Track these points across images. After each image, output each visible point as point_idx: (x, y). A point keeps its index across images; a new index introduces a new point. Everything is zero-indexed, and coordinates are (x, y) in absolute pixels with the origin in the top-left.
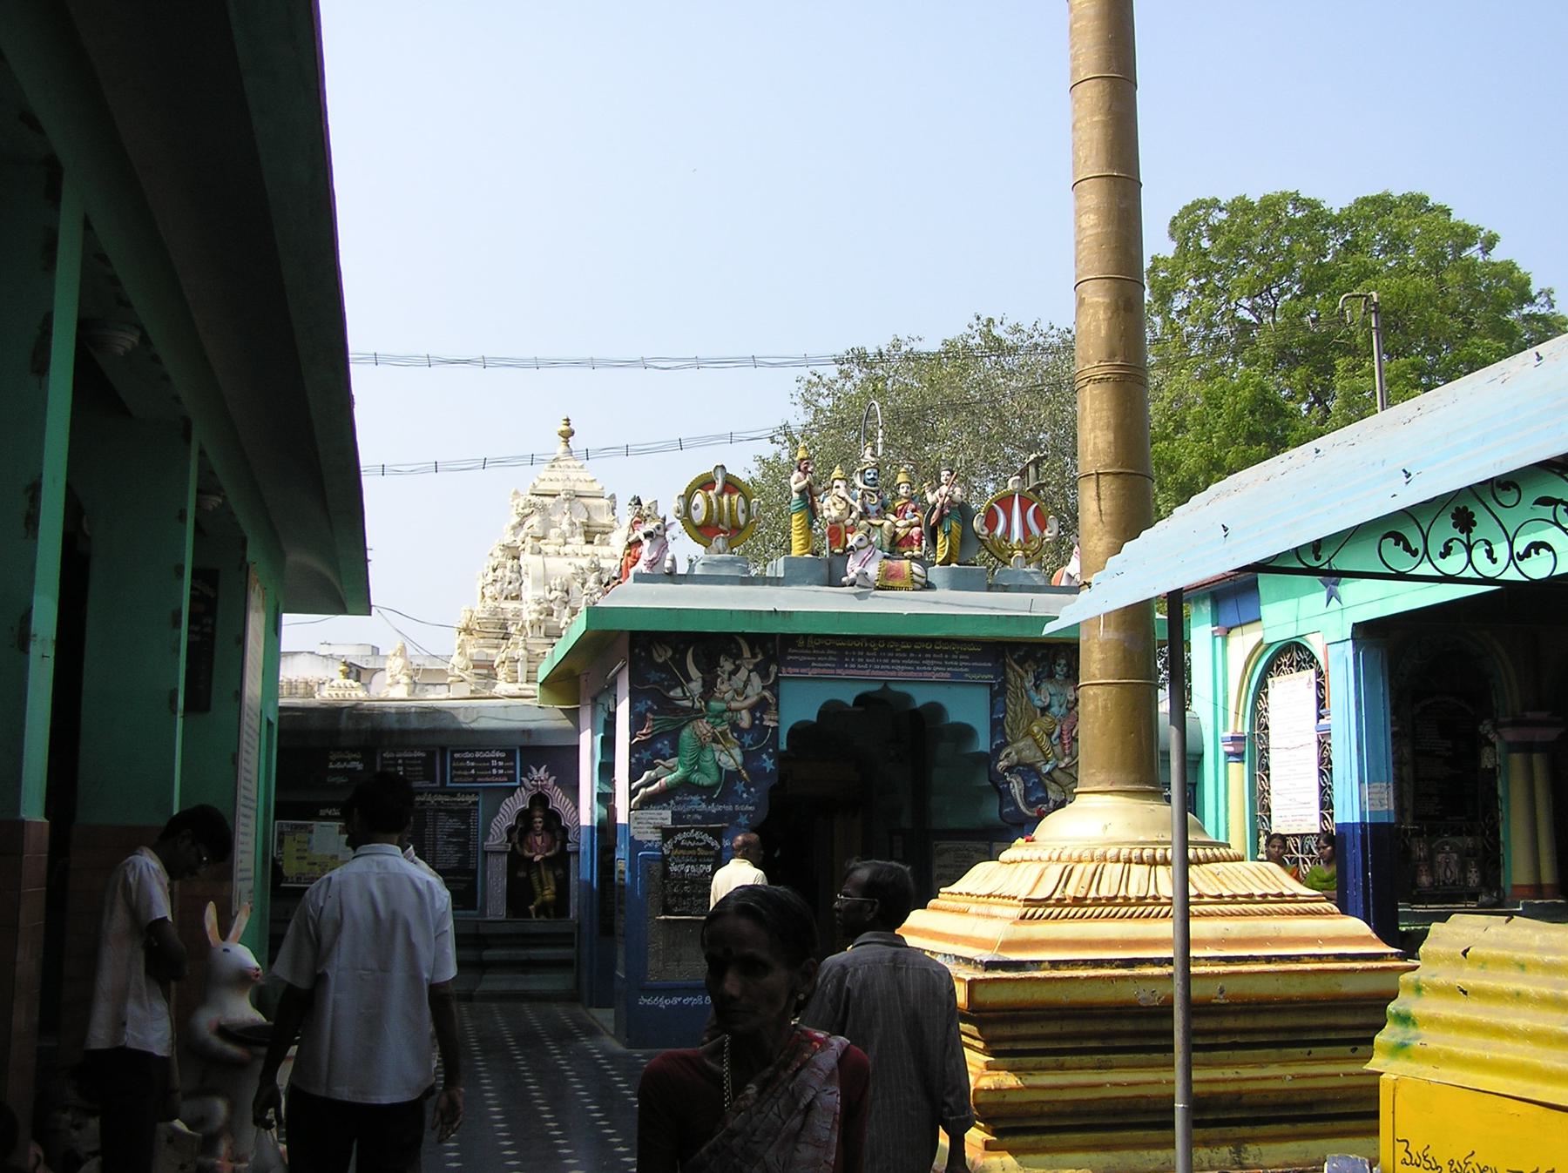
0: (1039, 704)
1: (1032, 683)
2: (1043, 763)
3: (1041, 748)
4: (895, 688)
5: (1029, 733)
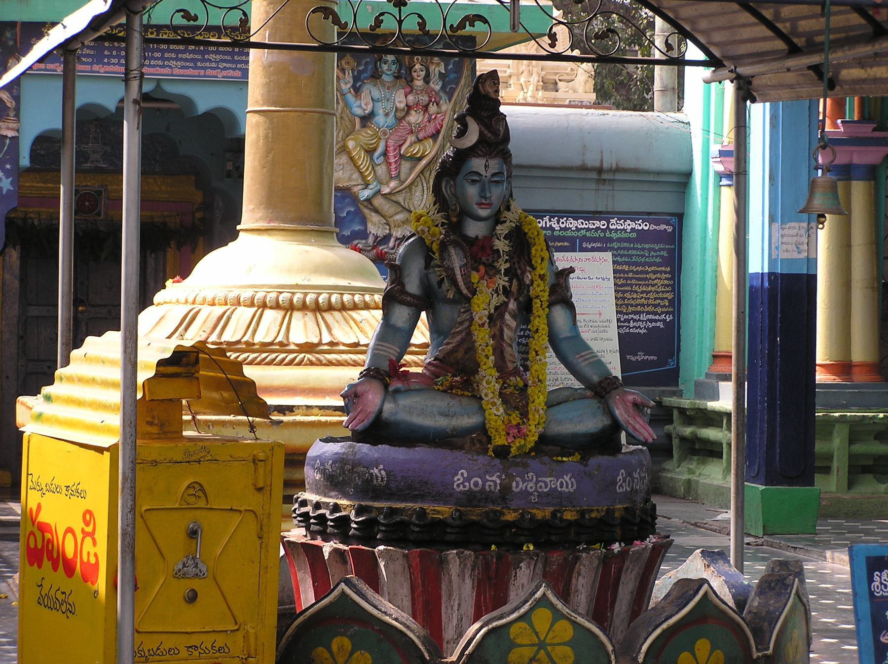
0: (359, 112)
1: (349, 85)
2: (360, 187)
3: (358, 168)
4: (171, 89)
5: (344, 149)
